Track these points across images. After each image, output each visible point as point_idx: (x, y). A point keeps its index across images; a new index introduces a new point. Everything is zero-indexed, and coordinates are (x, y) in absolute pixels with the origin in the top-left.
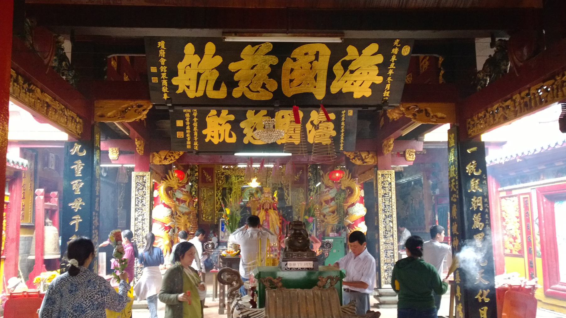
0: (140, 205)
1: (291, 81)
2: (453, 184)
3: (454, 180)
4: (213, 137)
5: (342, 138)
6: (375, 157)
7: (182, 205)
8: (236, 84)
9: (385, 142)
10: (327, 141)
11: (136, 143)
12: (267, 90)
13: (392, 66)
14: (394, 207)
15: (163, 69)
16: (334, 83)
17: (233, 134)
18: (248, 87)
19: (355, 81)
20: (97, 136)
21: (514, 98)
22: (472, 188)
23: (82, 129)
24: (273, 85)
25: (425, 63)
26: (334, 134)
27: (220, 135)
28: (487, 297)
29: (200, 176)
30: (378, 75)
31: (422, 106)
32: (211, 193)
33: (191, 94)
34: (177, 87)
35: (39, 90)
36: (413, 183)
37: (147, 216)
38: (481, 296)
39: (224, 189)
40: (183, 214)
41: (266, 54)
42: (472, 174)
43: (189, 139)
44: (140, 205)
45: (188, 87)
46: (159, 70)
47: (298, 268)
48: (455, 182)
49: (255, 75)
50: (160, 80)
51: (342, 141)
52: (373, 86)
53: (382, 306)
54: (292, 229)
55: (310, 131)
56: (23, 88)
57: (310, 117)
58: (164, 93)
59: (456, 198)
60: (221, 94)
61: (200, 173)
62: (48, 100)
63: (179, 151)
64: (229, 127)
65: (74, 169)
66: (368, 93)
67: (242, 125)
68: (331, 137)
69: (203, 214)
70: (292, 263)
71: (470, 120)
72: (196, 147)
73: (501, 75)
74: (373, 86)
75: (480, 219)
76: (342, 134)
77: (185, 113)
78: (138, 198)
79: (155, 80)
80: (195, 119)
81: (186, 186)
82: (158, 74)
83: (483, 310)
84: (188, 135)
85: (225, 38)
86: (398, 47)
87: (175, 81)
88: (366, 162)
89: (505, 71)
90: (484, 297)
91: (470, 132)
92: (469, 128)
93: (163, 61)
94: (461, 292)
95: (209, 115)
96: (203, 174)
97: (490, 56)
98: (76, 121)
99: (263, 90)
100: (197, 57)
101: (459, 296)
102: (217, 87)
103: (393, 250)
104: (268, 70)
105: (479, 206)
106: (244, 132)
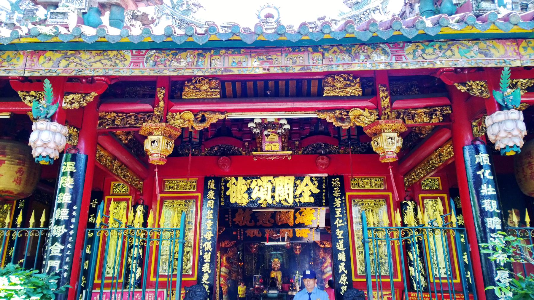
8: (258, 221)
15: (230, 215)
33: (240, 224)
34: (235, 222)
50: (229, 219)
58: (209, 190)
60: (253, 223)
82: (228, 218)
87: (234, 220)
93: (230, 213)
102: (250, 222)
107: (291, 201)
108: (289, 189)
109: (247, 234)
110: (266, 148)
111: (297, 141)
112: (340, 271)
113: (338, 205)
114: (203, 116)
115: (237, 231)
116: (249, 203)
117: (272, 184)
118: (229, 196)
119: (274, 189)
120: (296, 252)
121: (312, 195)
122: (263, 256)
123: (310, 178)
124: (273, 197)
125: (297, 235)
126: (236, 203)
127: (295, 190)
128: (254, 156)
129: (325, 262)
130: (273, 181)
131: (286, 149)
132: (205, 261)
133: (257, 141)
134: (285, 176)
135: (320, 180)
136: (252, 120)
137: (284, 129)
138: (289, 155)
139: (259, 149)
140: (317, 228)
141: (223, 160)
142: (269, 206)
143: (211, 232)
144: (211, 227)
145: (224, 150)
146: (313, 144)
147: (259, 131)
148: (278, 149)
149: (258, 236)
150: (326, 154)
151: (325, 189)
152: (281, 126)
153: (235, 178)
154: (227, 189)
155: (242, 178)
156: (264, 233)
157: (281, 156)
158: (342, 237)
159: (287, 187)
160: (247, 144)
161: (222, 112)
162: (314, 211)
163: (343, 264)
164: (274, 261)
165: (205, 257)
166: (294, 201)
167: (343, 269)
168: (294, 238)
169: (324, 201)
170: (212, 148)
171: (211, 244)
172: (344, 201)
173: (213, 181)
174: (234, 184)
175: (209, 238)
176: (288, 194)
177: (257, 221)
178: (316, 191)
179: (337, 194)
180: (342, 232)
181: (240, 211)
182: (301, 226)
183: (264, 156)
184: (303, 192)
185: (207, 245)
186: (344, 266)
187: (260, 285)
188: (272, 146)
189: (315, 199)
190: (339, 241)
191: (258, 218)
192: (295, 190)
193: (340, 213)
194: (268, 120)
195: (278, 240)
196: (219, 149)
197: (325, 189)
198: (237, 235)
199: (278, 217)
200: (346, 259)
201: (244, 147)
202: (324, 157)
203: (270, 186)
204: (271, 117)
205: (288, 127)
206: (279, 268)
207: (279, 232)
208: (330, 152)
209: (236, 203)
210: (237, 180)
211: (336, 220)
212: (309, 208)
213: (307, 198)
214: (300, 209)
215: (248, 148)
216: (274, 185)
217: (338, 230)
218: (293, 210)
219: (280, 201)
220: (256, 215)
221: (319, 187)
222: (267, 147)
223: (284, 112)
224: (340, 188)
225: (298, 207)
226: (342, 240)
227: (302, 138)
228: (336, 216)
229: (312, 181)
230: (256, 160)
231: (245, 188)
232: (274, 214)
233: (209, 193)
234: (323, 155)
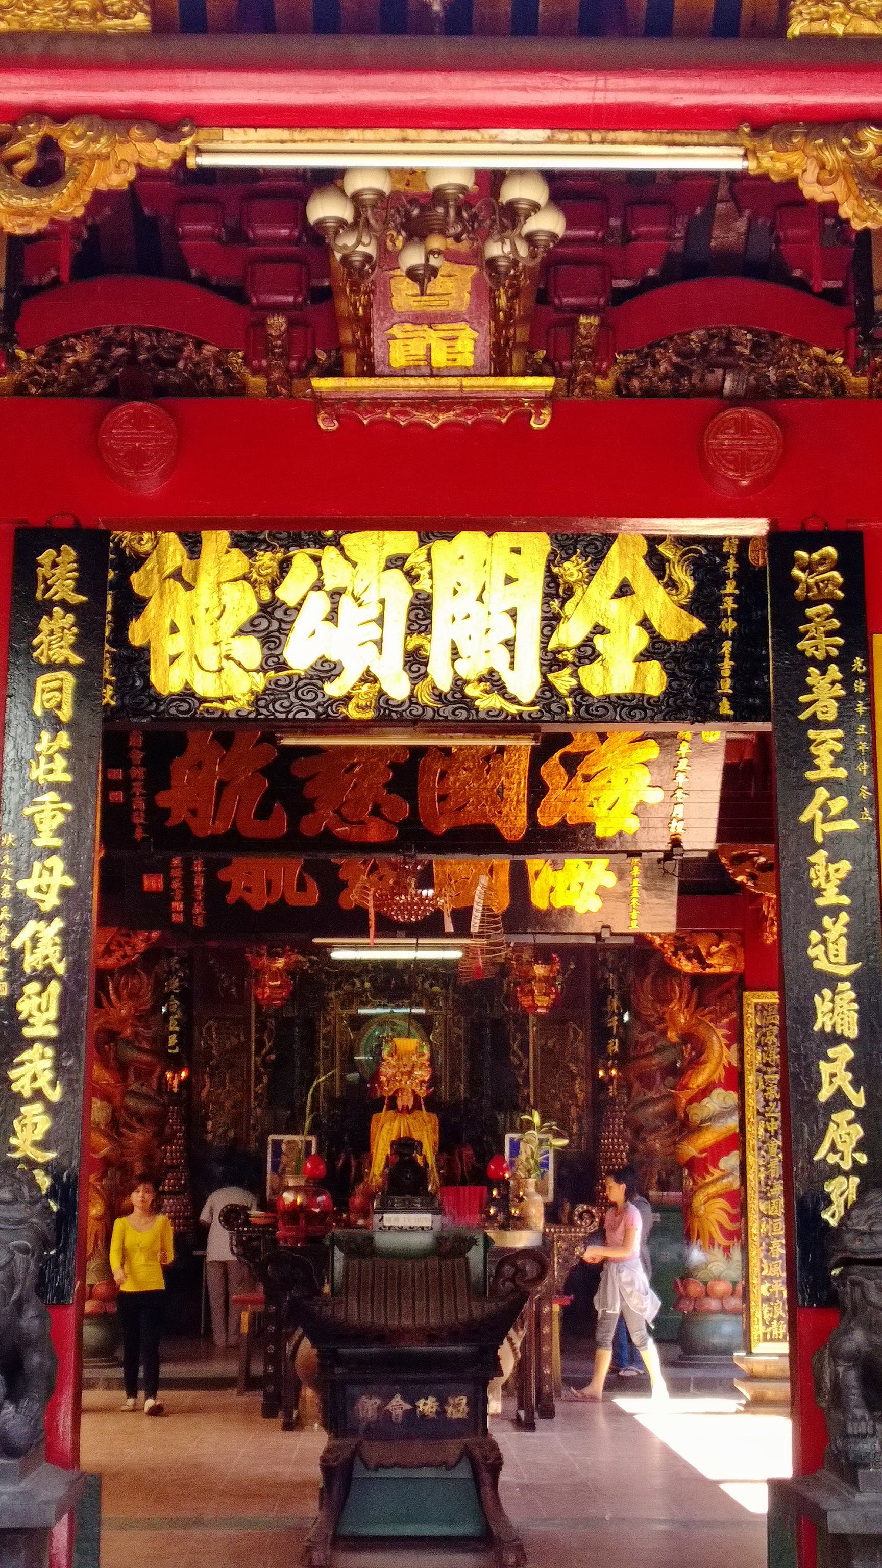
8: (309, 806)
15: (138, 772)
19: (597, 799)
32: (235, 1041)
34: (167, 812)
40: (140, 1121)
43: (178, 894)
50: (129, 796)
58: (46, 608)
60: (279, 823)
63: (151, 929)
84: (176, 884)
85: (282, 738)
87: (163, 799)
88: (710, 966)
93: (138, 756)
102: (264, 812)
107: (525, 683)
108: (513, 614)
109: (227, 886)
110: (398, 357)
111: (585, 310)
112: (824, 1095)
113: (828, 710)
114: (48, 146)
115: (164, 868)
116: (271, 693)
117: (412, 577)
118: (145, 650)
119: (421, 613)
120: (526, 1002)
121: (656, 649)
122: (310, 1026)
123: (644, 549)
124: (416, 661)
125: (539, 900)
126: (188, 694)
127: (551, 621)
128: (320, 401)
129: (696, 1062)
130: (417, 558)
131: (517, 360)
132: (27, 1032)
133: (343, 307)
134: (491, 529)
135: (706, 557)
136: (329, 179)
137: (530, 238)
138: (539, 403)
139: (351, 360)
140: (668, 856)
141: (131, 427)
142: (388, 715)
143: (57, 863)
144: (60, 832)
145: (131, 360)
146: (684, 335)
147: (371, 250)
148: (467, 360)
149: (296, 899)
150: (755, 396)
151: (736, 615)
152: (512, 214)
153: (183, 538)
154: (132, 605)
155: (224, 536)
156: (333, 886)
157: (487, 402)
158: (845, 900)
159: (500, 598)
160: (278, 323)
161: (167, 122)
162: (651, 751)
163: (844, 1053)
164: (394, 1052)
165: (24, 1007)
166: (547, 686)
167: (845, 1080)
168: (521, 913)
169: (726, 686)
170: (53, 357)
171: (64, 933)
172: (860, 686)
173: (69, 553)
174: (177, 575)
175: (51, 901)
176: (509, 644)
177: (300, 806)
178: (680, 626)
179: (824, 641)
180: (845, 866)
181: (200, 744)
182: (572, 839)
183: (385, 403)
184: (600, 630)
185: (35, 940)
186: (850, 1067)
187: (311, 1189)
188: (432, 344)
189: (671, 675)
190: (827, 921)
191: (310, 791)
192: (551, 621)
193: (838, 760)
194: (434, 183)
195: (430, 926)
196: (103, 353)
197: (736, 615)
198: (166, 896)
199: (430, 784)
200: (861, 1024)
201: (257, 344)
202: (753, 415)
203: (399, 594)
204: (450, 161)
205: (549, 223)
206: (422, 1092)
207: (426, 880)
208: (786, 388)
209: (188, 694)
210: (194, 548)
211: (811, 796)
212: (622, 734)
213: (622, 670)
214: (567, 739)
215: (286, 355)
216: (424, 584)
217: (819, 857)
218: (526, 743)
219: (459, 683)
220: (299, 769)
221: (702, 604)
222: (402, 347)
223: (541, 134)
224: (840, 609)
225: (559, 731)
226: (844, 917)
227: (621, 296)
228: (811, 775)
229: (657, 564)
230: (334, 426)
231: (244, 603)
232: (407, 770)
233: (45, 624)
234: (735, 400)
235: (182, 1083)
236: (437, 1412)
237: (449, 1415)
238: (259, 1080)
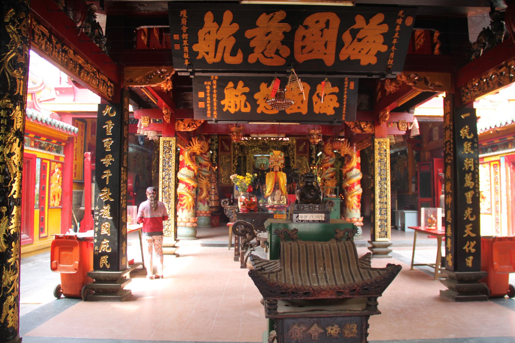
0: (167, 166)
1: (303, 47)
2: (448, 147)
3: (449, 143)
4: (230, 107)
5: (344, 109)
6: (373, 127)
7: (204, 169)
8: (252, 50)
9: (382, 114)
10: (330, 112)
11: (164, 112)
12: (280, 56)
13: (396, 35)
14: (389, 171)
16: (343, 51)
17: (247, 104)
18: (262, 53)
19: (362, 49)
20: (126, 100)
21: (509, 64)
22: (465, 150)
23: (113, 92)
24: (285, 51)
25: (420, 40)
26: (337, 105)
27: (236, 105)
28: (473, 248)
29: (220, 147)
30: (383, 44)
31: (423, 74)
34: (197, 53)
35: (72, 52)
36: (399, 153)
37: (173, 176)
38: (468, 247)
39: (239, 157)
40: (205, 177)
41: (279, 22)
42: (465, 137)
43: (209, 109)
44: (167, 166)
45: (207, 53)
46: (181, 37)
47: (309, 220)
48: (450, 145)
49: (269, 42)
50: (182, 47)
51: (344, 112)
52: (379, 54)
53: (375, 256)
54: (303, 181)
55: (316, 103)
56: (56, 48)
57: (316, 90)
59: (450, 159)
60: (238, 59)
61: (220, 143)
62: (80, 62)
64: (244, 98)
65: (106, 128)
66: (373, 61)
67: (256, 96)
68: (335, 108)
69: (222, 177)
70: (303, 215)
71: (464, 88)
72: (216, 116)
73: (496, 44)
74: (379, 54)
75: (471, 178)
76: (345, 106)
77: (206, 85)
78: (165, 160)
79: (177, 47)
80: (215, 91)
81: (208, 153)
82: (180, 41)
83: (469, 259)
84: (208, 105)
86: (402, 18)
87: (195, 48)
88: (365, 131)
89: (500, 41)
90: (471, 248)
91: (464, 99)
92: (463, 96)
93: (184, 29)
94: (451, 244)
95: (227, 88)
96: (222, 144)
97: (484, 28)
98: (107, 85)
99: (276, 56)
100: (215, 24)
101: (449, 247)
102: (233, 53)
103: (387, 209)
104: (281, 36)
105: (471, 167)
106: (258, 103)
109: (224, 106)
122: (245, 158)
149: (244, 110)
191: (252, 44)
235: (216, 170)
236: (339, 334)
237: (346, 335)
238: (234, 168)
